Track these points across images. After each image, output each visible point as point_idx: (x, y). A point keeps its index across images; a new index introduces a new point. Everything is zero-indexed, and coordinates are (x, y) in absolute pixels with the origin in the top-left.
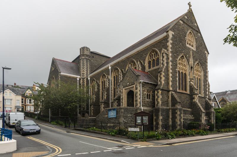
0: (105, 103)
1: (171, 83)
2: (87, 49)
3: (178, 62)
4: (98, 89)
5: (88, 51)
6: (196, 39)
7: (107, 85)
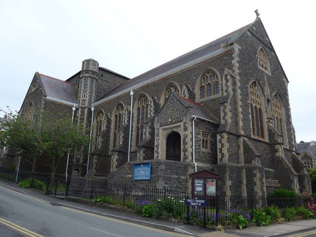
0: (119, 152)
1: (241, 124)
2: (95, 63)
3: (250, 90)
4: (108, 127)
5: (95, 65)
6: (270, 59)
7: (126, 121)
